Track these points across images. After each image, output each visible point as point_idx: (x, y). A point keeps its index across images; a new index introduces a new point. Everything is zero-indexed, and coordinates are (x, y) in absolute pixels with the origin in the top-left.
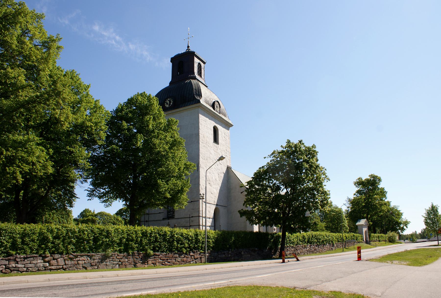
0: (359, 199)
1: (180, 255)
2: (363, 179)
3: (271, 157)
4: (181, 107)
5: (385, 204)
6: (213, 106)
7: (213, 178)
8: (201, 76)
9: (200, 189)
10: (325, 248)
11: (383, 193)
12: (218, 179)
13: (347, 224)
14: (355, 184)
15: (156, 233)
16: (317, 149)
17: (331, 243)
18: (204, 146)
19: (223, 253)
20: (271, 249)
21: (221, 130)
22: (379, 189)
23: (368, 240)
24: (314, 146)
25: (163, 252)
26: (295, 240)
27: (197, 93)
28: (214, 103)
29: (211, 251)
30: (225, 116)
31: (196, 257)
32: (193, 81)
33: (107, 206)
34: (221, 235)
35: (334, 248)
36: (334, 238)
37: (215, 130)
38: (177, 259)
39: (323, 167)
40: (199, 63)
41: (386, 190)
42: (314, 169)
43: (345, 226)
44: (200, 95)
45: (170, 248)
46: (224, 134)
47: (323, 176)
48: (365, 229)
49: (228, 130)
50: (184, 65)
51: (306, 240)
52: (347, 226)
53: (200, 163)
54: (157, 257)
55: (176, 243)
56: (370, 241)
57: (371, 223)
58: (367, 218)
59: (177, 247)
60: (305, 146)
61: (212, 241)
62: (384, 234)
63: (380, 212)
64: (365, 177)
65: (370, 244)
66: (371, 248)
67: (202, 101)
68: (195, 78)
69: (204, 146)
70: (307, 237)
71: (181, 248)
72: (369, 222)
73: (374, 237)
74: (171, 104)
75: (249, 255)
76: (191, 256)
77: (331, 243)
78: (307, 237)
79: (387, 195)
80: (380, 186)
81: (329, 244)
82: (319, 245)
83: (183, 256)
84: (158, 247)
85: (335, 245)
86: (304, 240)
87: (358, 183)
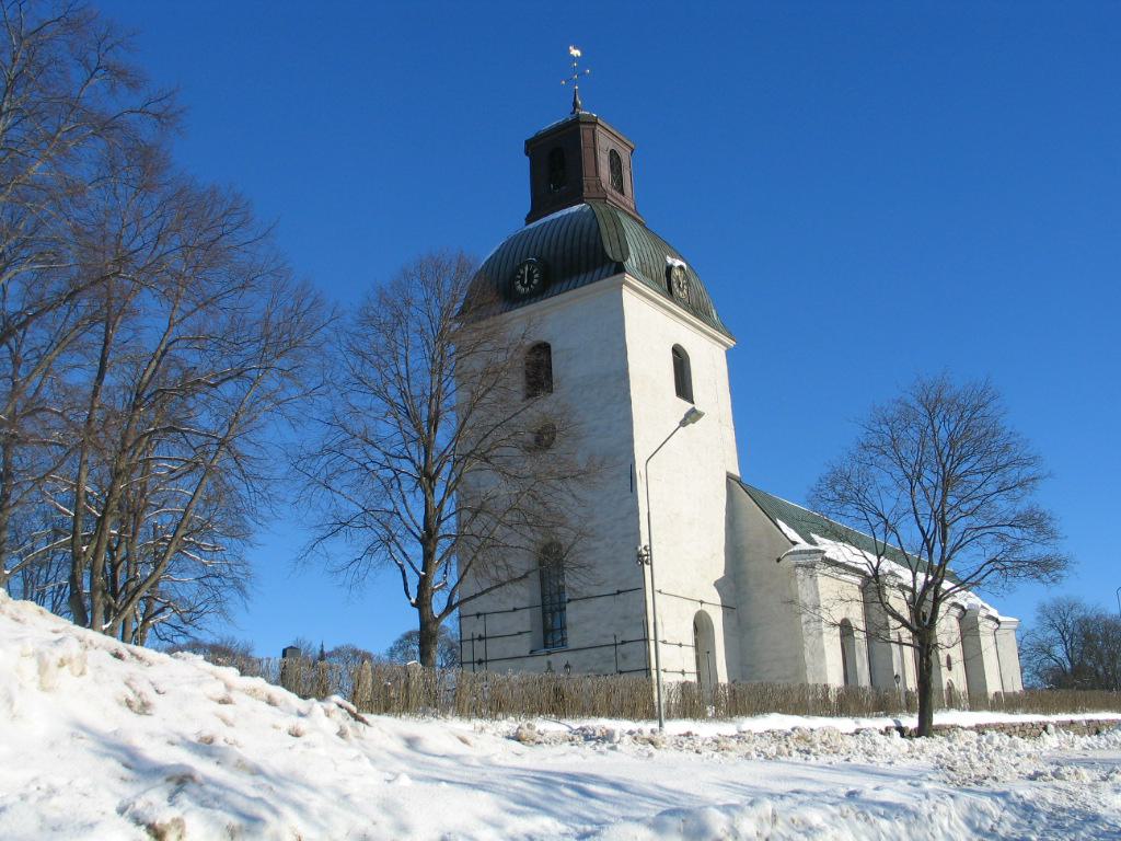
74: (535, 281)
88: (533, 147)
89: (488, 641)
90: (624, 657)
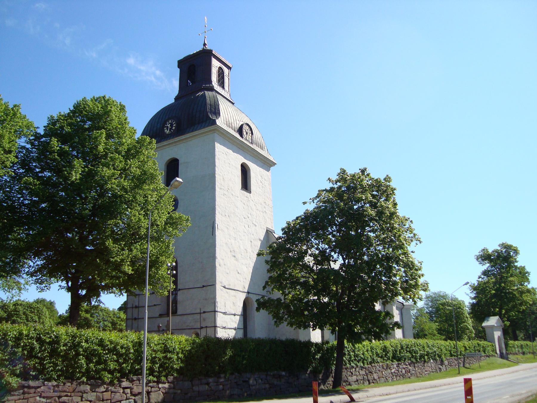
0: (485, 283)
1: (93, 388)
2: (490, 251)
3: (315, 201)
4: (188, 133)
5: (528, 291)
6: (240, 131)
7: (242, 247)
8: (223, 87)
9: (217, 265)
10: (427, 368)
11: (523, 275)
12: (249, 250)
13: (471, 325)
14: (477, 259)
15: (32, 338)
16: (393, 184)
17: (438, 357)
18: (224, 195)
19: (204, 381)
20: (315, 372)
21: (255, 170)
22: (516, 267)
23: (504, 352)
24: (388, 179)
25: (49, 380)
26: (368, 355)
27: (213, 109)
28: (241, 127)
29: (175, 378)
30: (262, 148)
31: (136, 390)
32: (208, 94)
33: (42, 290)
34: (201, 345)
35: (443, 368)
36: (444, 350)
37: (245, 171)
38: (85, 395)
39: (407, 217)
40: (220, 68)
41: (528, 269)
42: (387, 218)
43: (468, 329)
44: (217, 113)
45: (67, 370)
46: (260, 177)
47: (408, 235)
48: (497, 334)
49: (268, 170)
50: (196, 69)
51: (390, 355)
52: (470, 327)
53: (217, 222)
54: (32, 391)
55: (83, 361)
56: (507, 354)
57: (508, 323)
58: (500, 314)
59: (88, 370)
60: (371, 179)
61: (178, 358)
62: (530, 341)
63: (521, 304)
64: (493, 247)
65: (507, 359)
66: (509, 367)
67: (219, 122)
68: (212, 89)
69: (224, 195)
70: (391, 349)
71: (97, 371)
72: (503, 322)
73: (514, 347)
74: (174, 128)
75: (267, 386)
76: (124, 388)
77: (438, 357)
78: (391, 349)
79: (531, 278)
80: (518, 264)
81: (435, 360)
82: (414, 363)
83: (102, 389)
84: (35, 369)
85: (446, 362)
86: (386, 355)
87: (481, 256)
88: (182, 64)
89: (140, 309)
90: (204, 320)
